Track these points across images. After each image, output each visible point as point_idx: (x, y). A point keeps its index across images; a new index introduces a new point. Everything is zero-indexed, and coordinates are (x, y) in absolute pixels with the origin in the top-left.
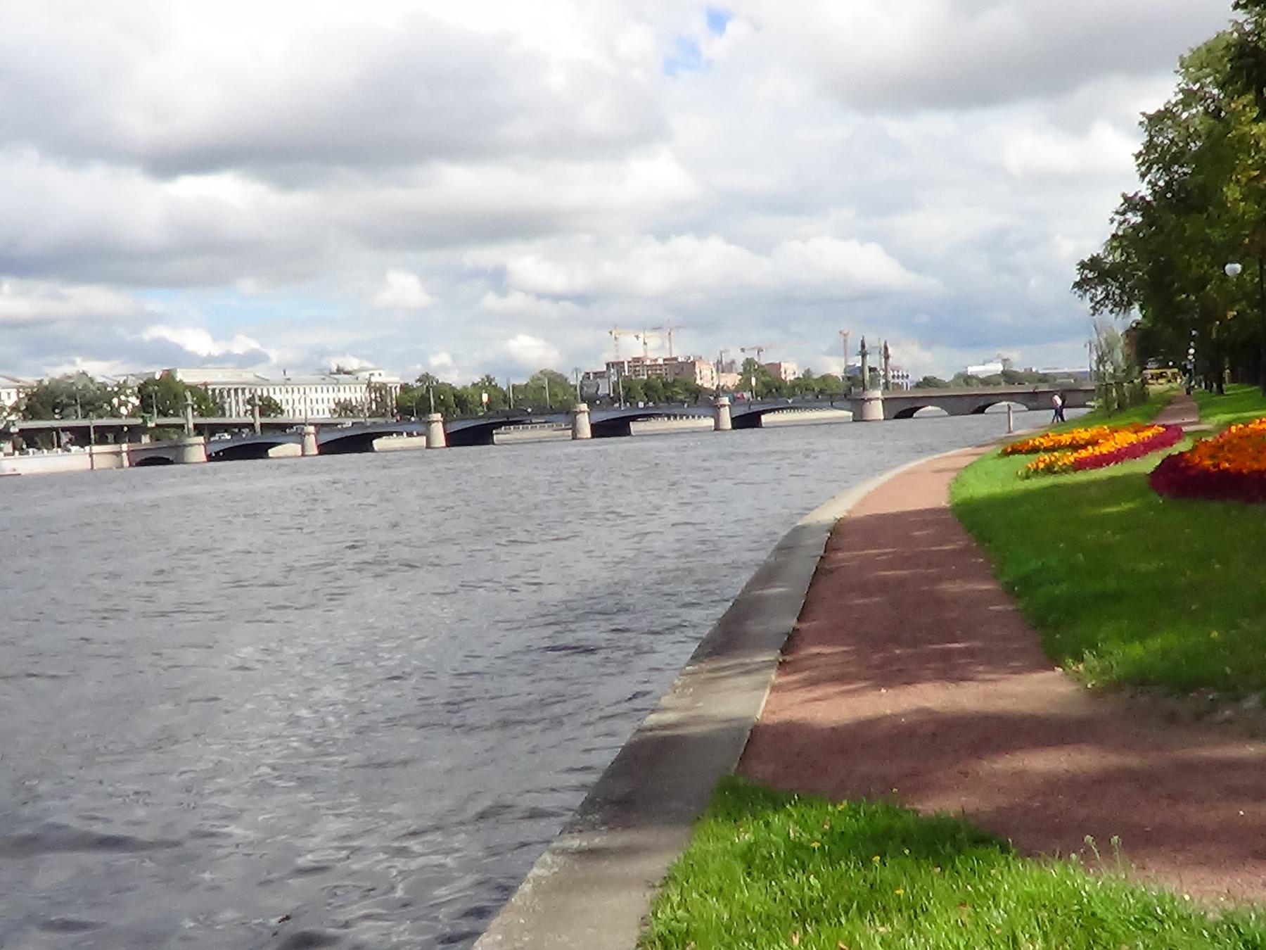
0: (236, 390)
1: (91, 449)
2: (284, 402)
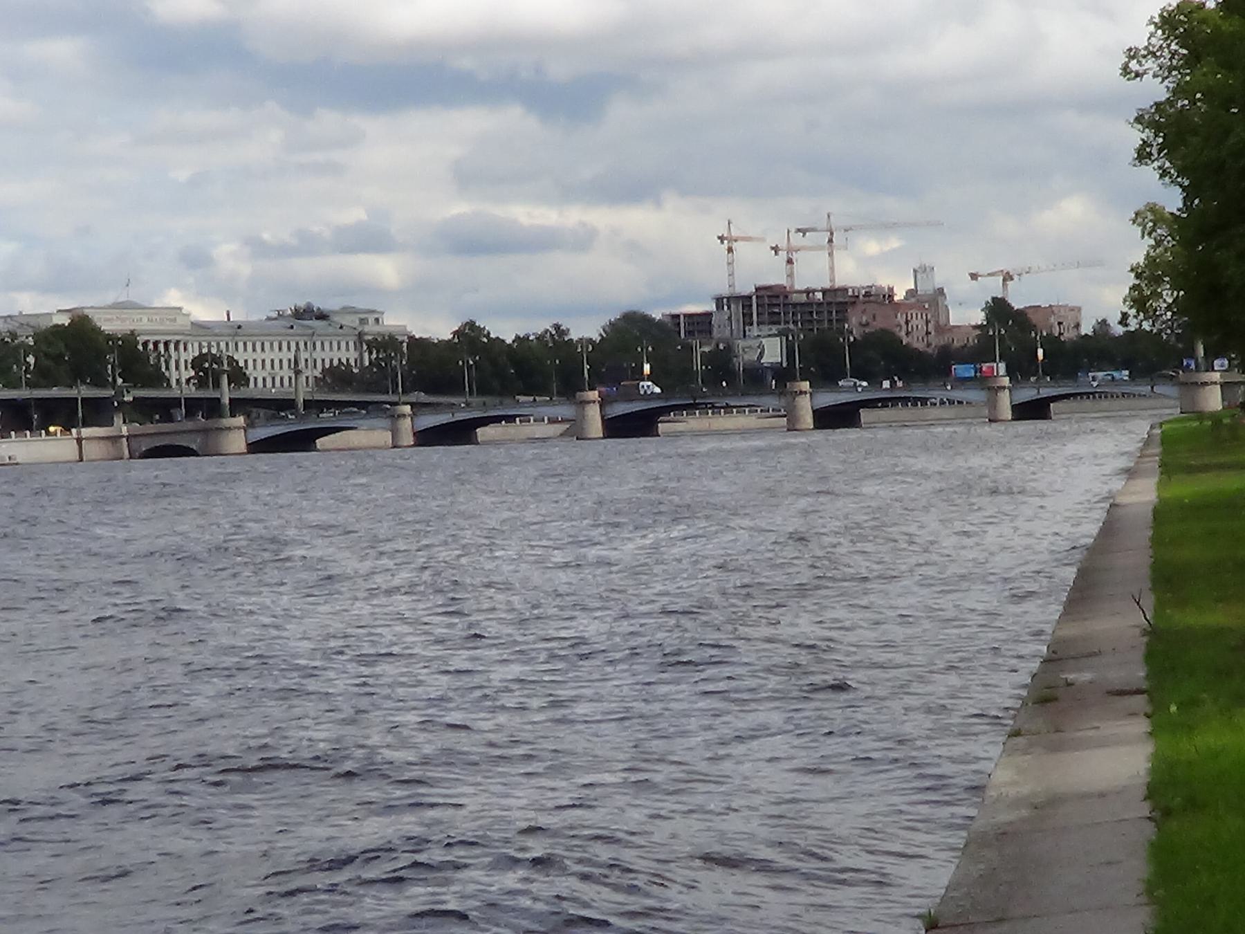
0: (166, 344)
1: (79, 433)
2: (250, 363)
